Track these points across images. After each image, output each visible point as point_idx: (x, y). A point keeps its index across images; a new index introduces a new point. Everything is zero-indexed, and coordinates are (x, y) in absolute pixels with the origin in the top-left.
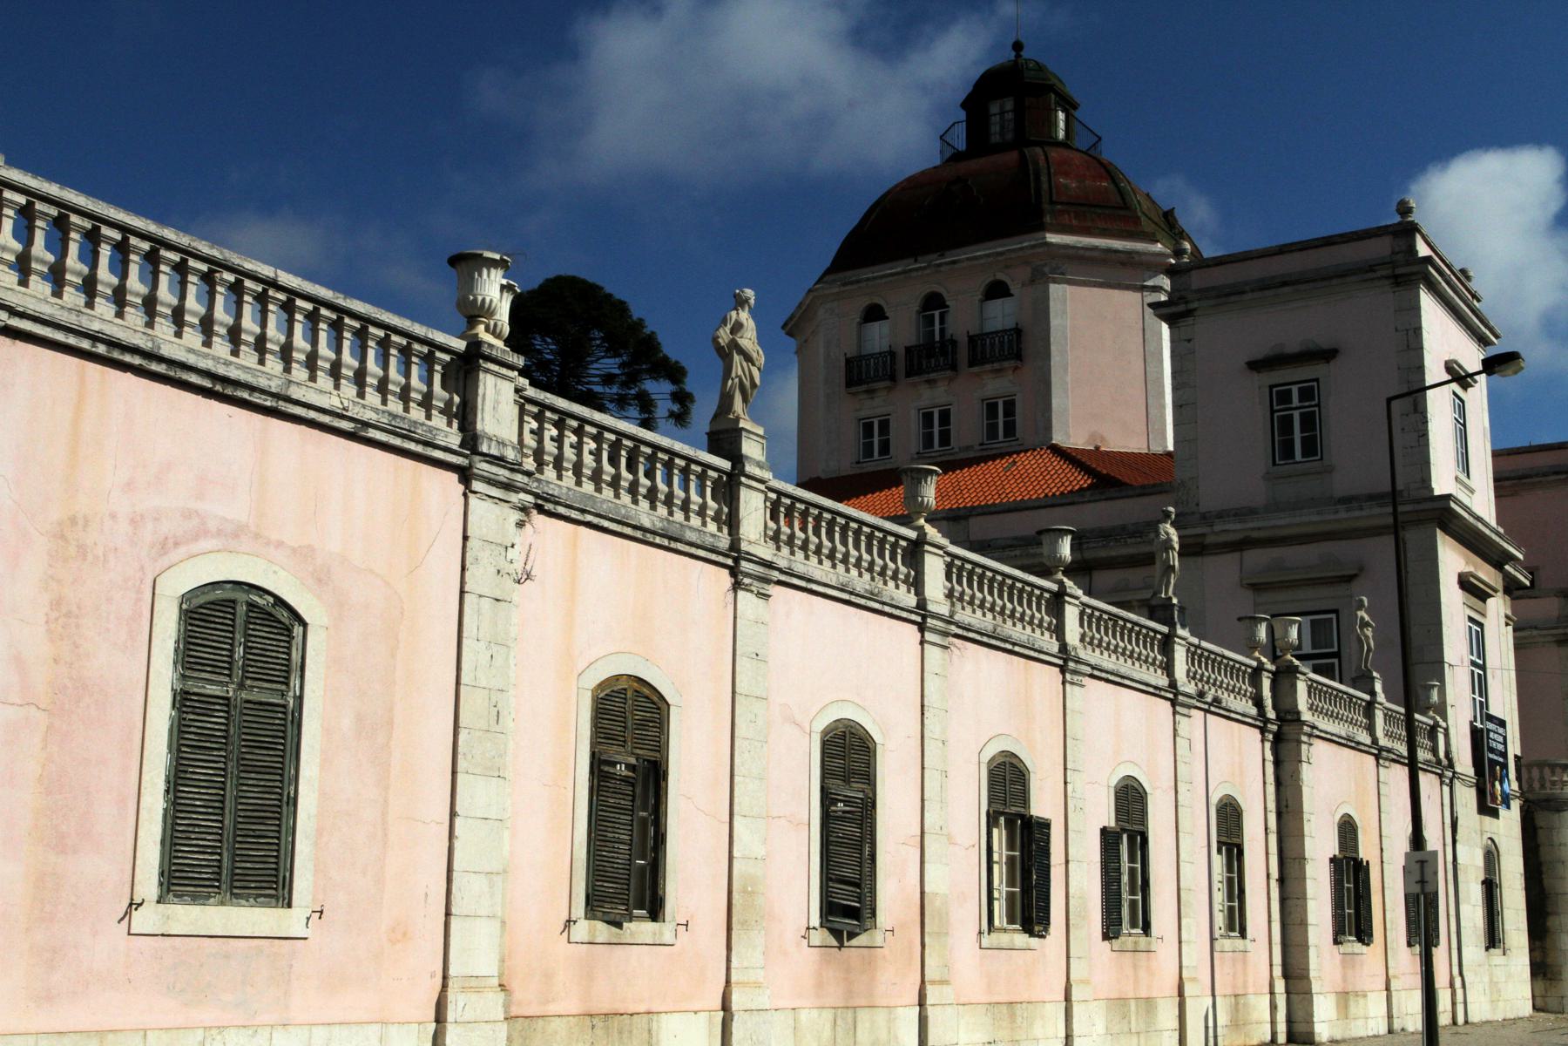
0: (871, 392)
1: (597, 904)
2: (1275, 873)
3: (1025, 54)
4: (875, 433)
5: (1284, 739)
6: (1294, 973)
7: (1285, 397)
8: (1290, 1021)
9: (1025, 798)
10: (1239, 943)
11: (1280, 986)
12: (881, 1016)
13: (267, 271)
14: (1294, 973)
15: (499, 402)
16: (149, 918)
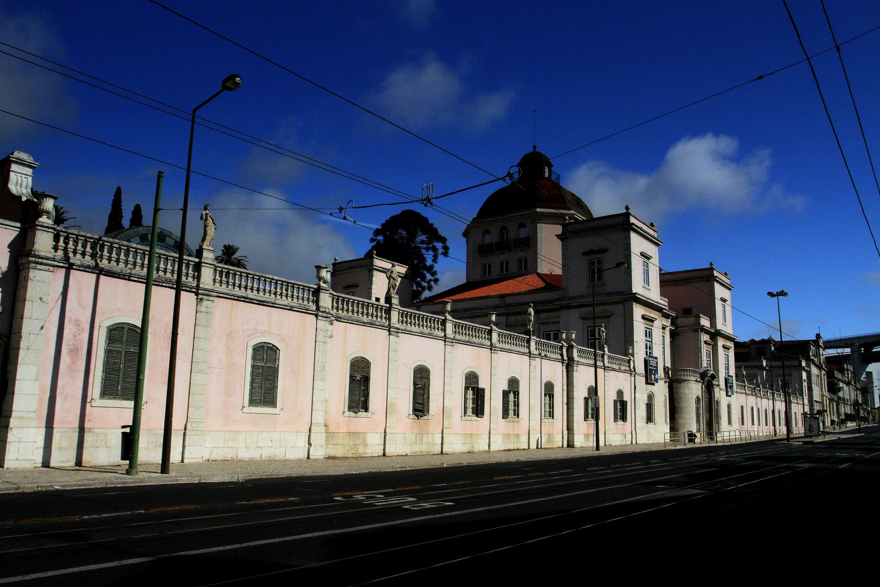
0: (486, 256)
1: (350, 408)
2: (565, 402)
3: (537, 150)
4: (487, 269)
5: (569, 365)
6: (570, 428)
7: (593, 263)
8: (568, 441)
9: (477, 383)
10: (551, 420)
11: (565, 432)
12: (430, 436)
13: (271, 277)
14: (570, 428)
15: (326, 300)
16: (246, 409)
